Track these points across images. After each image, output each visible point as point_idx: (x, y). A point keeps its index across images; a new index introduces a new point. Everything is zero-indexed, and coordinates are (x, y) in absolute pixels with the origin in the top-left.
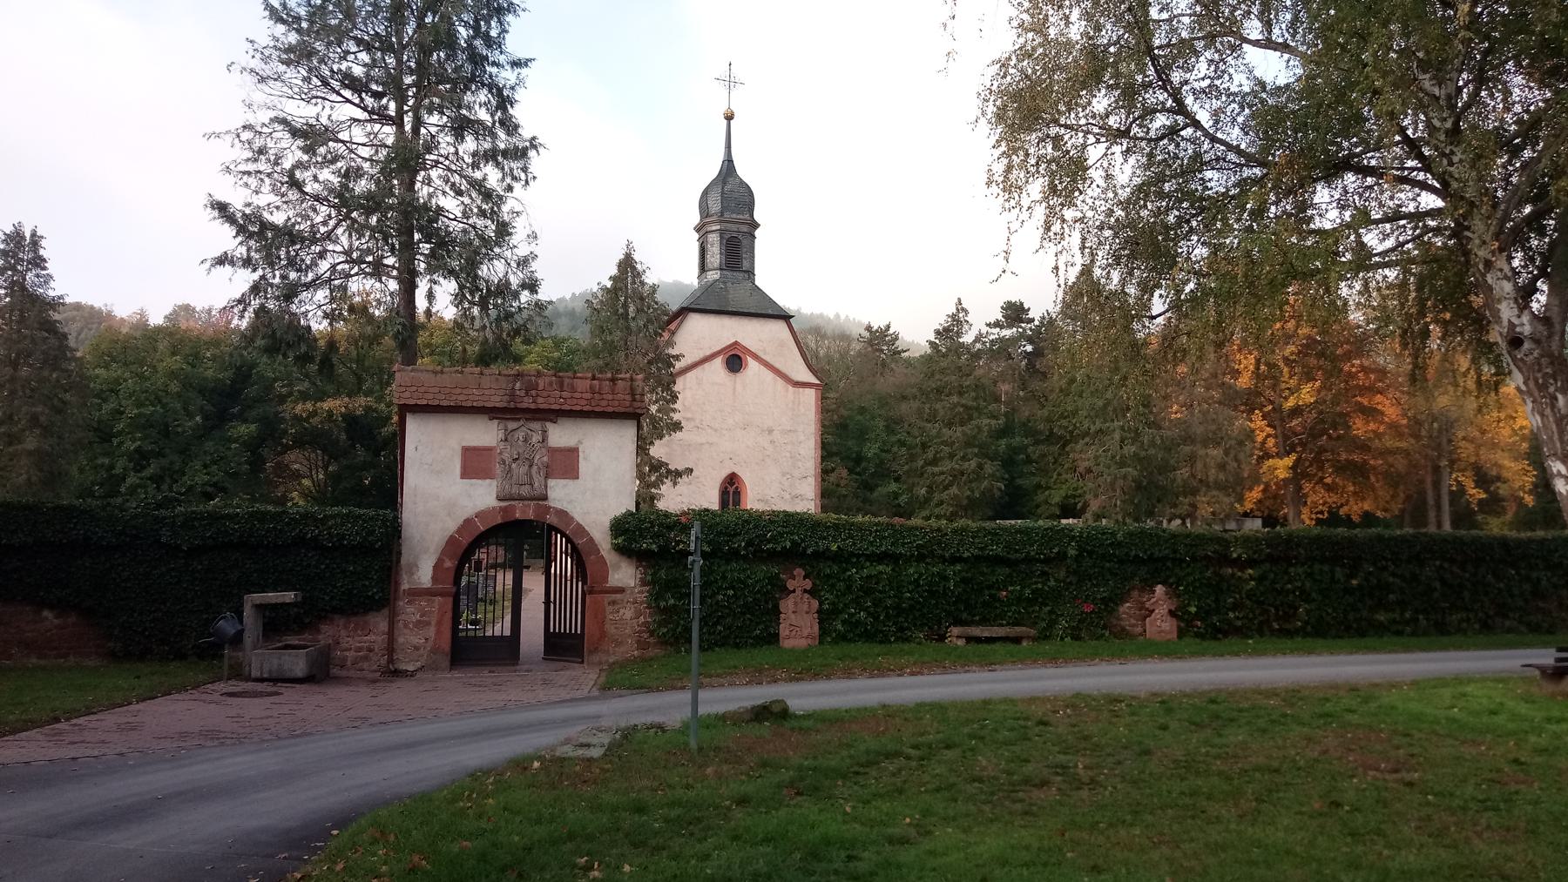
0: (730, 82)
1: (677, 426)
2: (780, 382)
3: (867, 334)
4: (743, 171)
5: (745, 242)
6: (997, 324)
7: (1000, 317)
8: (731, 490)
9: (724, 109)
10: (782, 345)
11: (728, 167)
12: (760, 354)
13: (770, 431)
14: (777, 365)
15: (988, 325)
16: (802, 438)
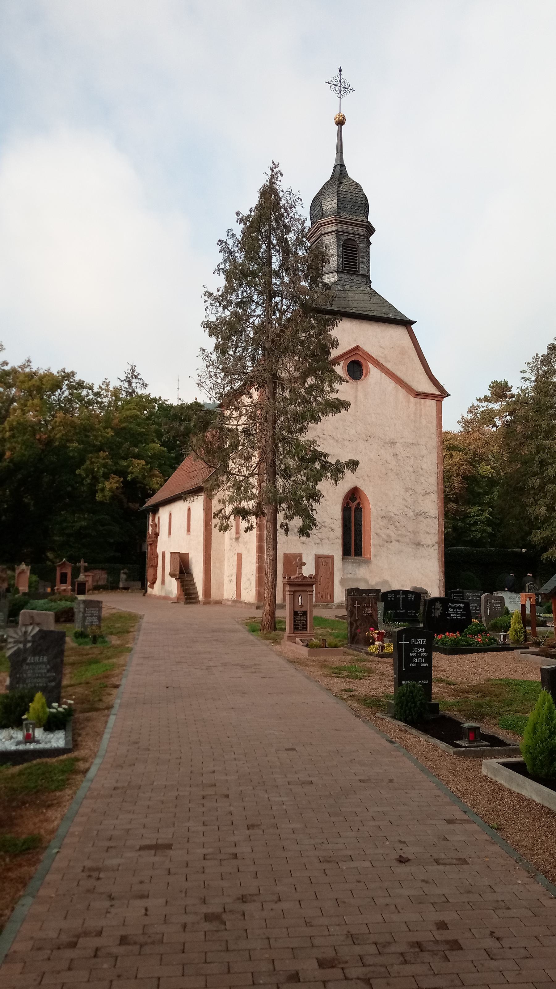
0: (341, 87)
1: (308, 536)
2: (402, 392)
3: (114, 681)
4: (354, 173)
5: (362, 245)
6: (486, 399)
7: (489, 394)
8: (353, 506)
9: (335, 113)
10: (403, 352)
11: (340, 173)
12: (382, 361)
13: (393, 444)
14: (399, 374)
15: (480, 400)
16: (424, 452)
